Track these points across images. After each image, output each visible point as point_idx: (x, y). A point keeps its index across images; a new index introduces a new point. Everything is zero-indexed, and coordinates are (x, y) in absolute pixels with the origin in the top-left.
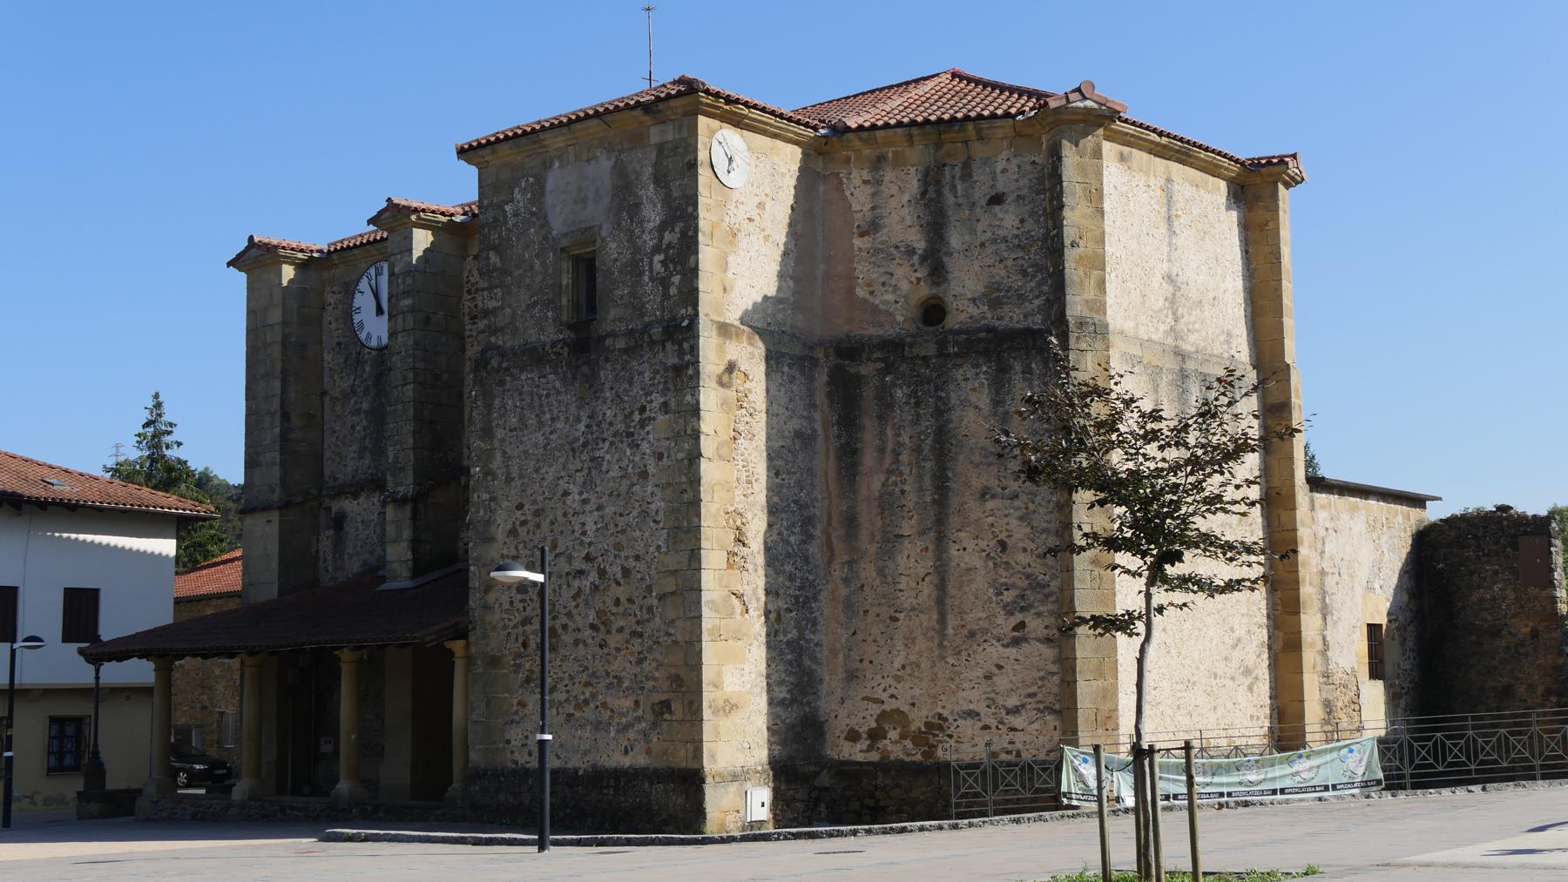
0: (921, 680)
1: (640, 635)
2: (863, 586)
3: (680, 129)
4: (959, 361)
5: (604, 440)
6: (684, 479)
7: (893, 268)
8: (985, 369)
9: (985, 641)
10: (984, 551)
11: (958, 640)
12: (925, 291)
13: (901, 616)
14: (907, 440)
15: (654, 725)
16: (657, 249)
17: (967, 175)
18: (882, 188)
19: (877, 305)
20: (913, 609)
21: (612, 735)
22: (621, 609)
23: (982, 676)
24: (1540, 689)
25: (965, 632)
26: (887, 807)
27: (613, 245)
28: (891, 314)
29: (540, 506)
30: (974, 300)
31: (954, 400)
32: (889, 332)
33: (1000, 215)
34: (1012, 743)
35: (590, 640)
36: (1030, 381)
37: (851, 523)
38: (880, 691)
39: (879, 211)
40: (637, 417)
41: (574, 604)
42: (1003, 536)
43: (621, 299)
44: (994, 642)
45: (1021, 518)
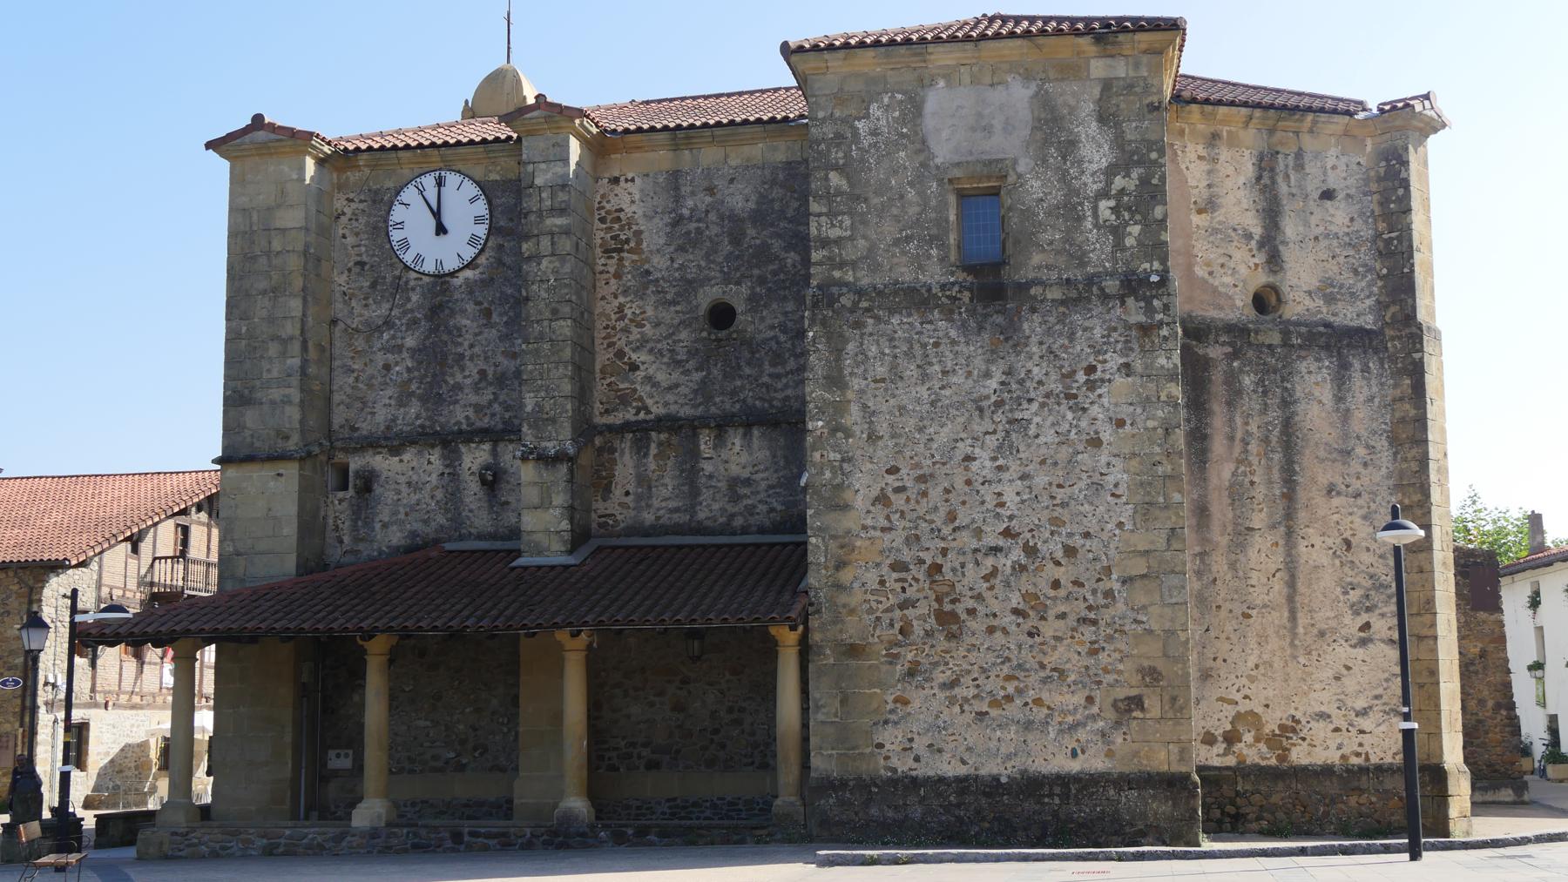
0: (1274, 680)
1: (1094, 622)
2: (1215, 580)
3: (1137, 66)
4: (1303, 353)
5: (1030, 401)
6: (1157, 449)
7: (1232, 250)
8: (1327, 364)
9: (1334, 641)
10: (1331, 548)
11: (1309, 640)
12: (1262, 278)
13: (1254, 613)
14: (1255, 430)
15: (1118, 723)
16: (1104, 194)
17: (1300, 167)
18: (1218, 166)
19: (1217, 287)
20: (1265, 606)
21: (1052, 735)
22: (1062, 593)
23: (1331, 677)
24: (1490, 704)
25: (1315, 631)
26: (1248, 814)
27: (1037, 184)
28: (1230, 298)
29: (926, 471)
30: (1310, 293)
31: (1299, 394)
32: (1231, 316)
33: (1332, 211)
34: (1361, 745)
35: (1014, 628)
36: (1368, 380)
37: (1202, 512)
38: (1235, 692)
39: (1215, 189)
40: (1081, 377)
41: (986, 585)
42: (1347, 534)
43: (1048, 245)
44: (1343, 642)
45: (1365, 518)
